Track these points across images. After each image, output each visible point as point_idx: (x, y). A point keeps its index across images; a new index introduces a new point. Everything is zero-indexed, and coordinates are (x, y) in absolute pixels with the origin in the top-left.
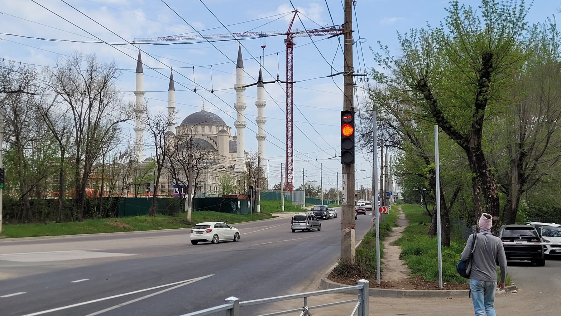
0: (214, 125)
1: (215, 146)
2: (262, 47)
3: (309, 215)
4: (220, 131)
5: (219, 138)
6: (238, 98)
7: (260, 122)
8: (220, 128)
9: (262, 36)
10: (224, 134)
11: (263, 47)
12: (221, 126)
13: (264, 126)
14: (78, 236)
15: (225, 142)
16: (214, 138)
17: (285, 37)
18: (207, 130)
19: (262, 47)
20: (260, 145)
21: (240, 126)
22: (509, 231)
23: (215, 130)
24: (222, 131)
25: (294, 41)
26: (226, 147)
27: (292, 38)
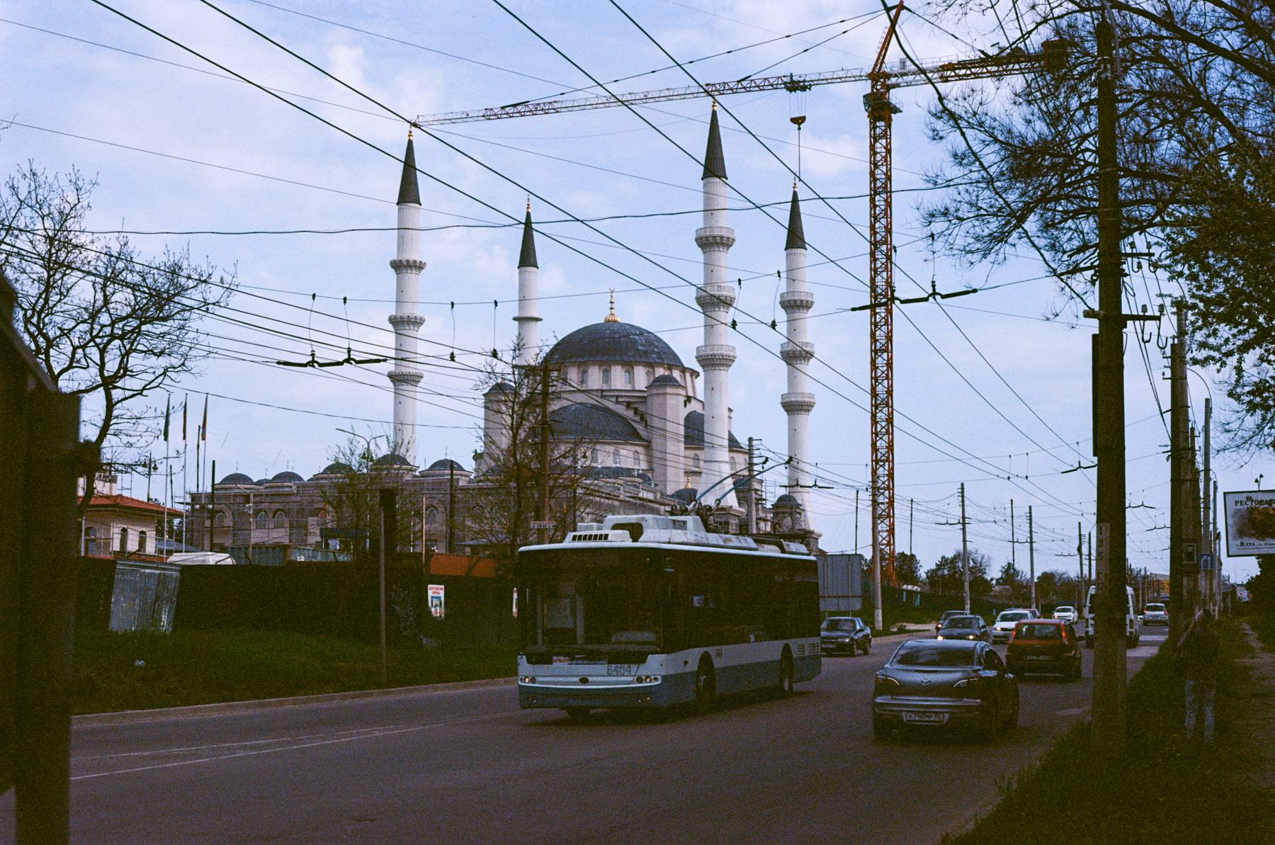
0: (639, 363)
1: (640, 428)
2: (794, 120)
3: (915, 218)
4: (656, 380)
5: (655, 402)
6: (792, 380)
7: (794, 356)
8: (660, 372)
9: (794, 86)
10: (669, 390)
11: (799, 121)
12: (661, 365)
13: (725, 258)
14: (376, 698)
15: (675, 411)
16: (638, 403)
17: (866, 87)
18: (619, 379)
19: (794, 120)
20: (793, 431)
21: (713, 361)
22: (620, 532)
23: (641, 378)
24: (667, 381)
25: (895, 96)
26: (678, 428)
27: (889, 88)
